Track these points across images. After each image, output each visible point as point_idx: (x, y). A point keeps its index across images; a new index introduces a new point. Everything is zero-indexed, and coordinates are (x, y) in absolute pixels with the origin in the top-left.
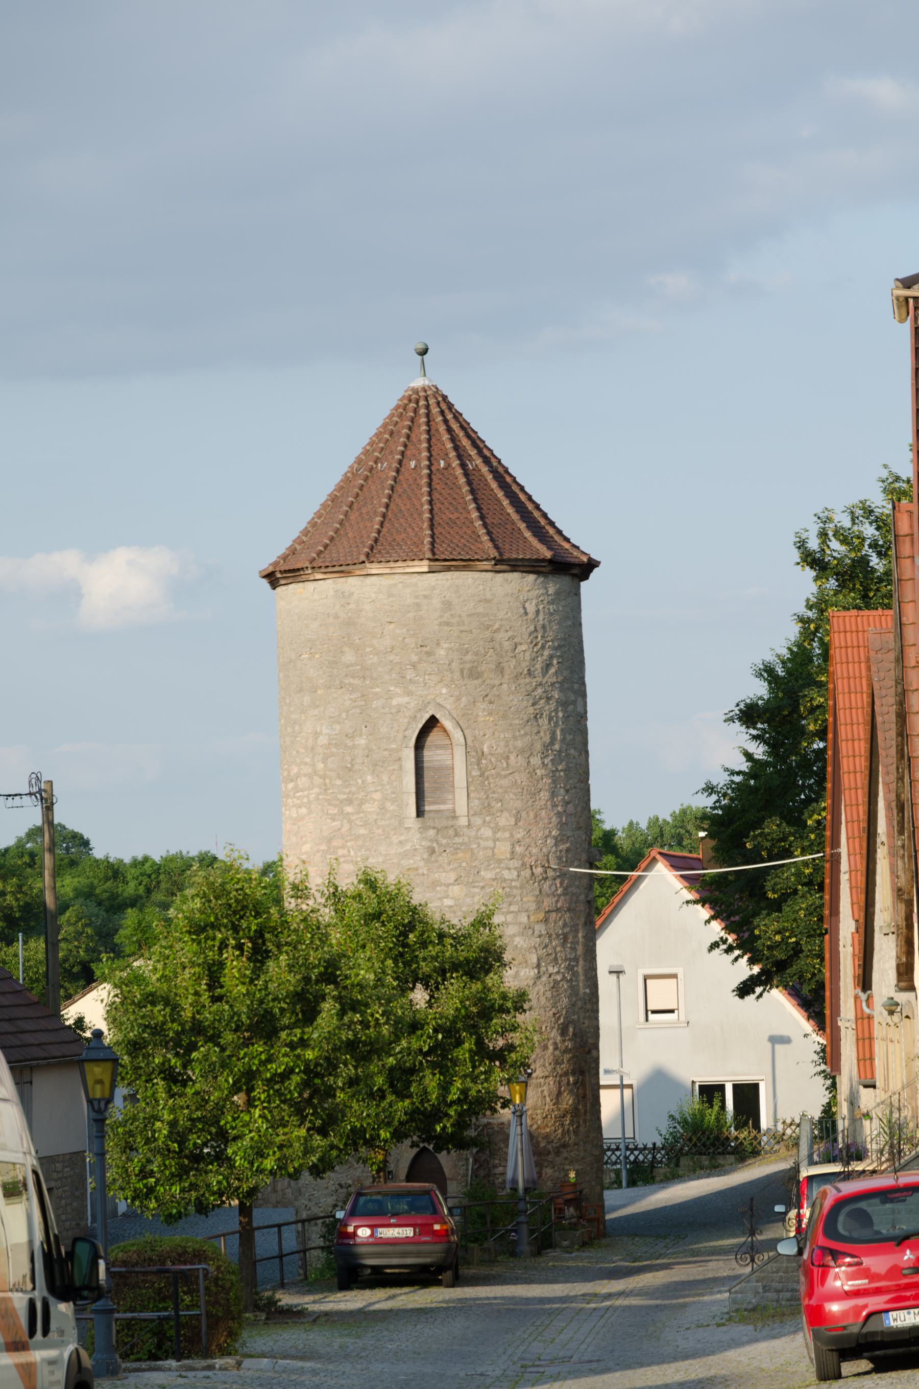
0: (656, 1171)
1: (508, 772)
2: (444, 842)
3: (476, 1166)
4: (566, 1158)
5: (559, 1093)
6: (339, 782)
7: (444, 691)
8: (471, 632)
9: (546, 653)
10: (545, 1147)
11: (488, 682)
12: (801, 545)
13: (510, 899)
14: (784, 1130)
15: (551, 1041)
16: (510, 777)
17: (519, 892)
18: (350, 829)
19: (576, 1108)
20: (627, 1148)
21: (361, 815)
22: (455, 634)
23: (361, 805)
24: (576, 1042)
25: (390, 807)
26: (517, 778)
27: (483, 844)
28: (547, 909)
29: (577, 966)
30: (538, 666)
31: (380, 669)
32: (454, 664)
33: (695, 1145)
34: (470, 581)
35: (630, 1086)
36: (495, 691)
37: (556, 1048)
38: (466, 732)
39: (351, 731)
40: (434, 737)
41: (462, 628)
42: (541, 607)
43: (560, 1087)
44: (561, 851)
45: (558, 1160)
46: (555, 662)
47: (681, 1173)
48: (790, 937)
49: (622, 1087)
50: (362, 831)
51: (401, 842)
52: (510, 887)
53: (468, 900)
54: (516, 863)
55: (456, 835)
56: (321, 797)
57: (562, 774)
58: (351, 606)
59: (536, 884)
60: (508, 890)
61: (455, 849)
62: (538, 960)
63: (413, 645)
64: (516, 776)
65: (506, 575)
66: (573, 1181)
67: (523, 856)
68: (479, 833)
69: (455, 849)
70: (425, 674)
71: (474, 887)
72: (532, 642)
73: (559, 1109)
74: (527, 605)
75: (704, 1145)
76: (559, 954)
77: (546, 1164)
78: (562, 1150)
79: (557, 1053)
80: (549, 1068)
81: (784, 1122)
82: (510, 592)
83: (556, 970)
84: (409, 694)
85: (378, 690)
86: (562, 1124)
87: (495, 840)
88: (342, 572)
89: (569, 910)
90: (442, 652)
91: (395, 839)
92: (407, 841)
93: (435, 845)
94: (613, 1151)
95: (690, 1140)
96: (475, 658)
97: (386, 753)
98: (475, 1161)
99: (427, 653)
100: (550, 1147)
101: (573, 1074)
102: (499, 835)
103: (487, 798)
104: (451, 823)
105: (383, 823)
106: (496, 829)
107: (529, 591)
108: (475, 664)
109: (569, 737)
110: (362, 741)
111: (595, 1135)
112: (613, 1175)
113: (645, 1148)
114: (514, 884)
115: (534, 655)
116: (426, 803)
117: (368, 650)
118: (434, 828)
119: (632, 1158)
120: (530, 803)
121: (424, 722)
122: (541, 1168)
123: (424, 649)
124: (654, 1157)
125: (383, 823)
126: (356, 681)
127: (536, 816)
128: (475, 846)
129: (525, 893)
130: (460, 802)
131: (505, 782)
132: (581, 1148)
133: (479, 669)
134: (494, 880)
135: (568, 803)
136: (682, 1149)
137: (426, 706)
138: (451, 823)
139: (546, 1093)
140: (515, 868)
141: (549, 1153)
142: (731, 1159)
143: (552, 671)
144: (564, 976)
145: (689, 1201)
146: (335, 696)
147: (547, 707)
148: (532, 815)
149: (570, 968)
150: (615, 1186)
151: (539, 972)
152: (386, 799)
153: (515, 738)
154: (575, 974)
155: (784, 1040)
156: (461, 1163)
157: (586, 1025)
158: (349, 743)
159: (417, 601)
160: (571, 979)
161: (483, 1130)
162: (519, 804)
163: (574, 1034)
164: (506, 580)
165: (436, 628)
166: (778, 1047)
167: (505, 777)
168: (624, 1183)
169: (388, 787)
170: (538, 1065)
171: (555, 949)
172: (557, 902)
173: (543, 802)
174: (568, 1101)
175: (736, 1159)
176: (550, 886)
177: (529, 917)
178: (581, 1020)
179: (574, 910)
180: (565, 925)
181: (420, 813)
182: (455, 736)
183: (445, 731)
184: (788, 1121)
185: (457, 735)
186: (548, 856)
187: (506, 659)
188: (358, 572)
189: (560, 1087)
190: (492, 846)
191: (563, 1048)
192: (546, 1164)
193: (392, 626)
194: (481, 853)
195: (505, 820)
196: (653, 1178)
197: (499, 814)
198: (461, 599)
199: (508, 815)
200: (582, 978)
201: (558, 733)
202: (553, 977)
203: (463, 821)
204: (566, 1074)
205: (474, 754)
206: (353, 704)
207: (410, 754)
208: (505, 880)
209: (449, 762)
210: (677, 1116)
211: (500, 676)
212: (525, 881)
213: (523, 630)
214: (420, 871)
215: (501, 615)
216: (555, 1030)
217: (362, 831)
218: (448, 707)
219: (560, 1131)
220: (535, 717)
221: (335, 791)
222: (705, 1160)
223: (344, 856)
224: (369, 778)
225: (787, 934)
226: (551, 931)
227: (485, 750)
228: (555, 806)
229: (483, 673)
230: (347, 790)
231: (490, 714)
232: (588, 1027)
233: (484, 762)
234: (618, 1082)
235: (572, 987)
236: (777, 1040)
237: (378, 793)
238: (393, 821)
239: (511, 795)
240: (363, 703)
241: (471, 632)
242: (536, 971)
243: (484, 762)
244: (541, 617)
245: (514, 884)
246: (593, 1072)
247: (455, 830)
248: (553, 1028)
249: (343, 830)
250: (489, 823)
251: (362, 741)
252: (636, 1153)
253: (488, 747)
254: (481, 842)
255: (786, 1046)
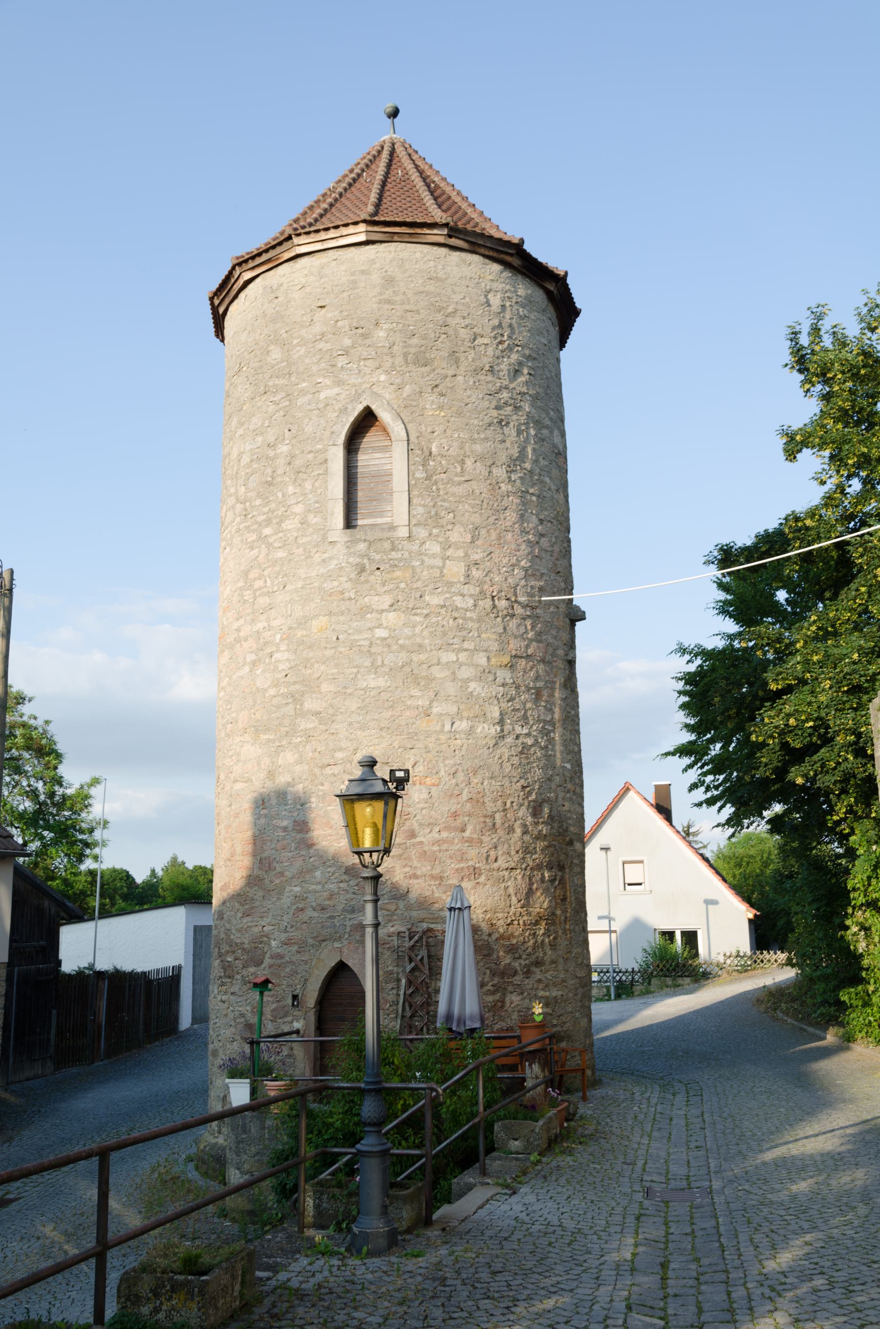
0: (634, 988)
1: (463, 479)
2: (377, 557)
3: (411, 991)
4: (540, 981)
5: (530, 892)
6: (258, 502)
7: (383, 378)
8: (418, 312)
9: (514, 357)
10: (509, 964)
11: (439, 371)
12: (794, 335)
13: (464, 633)
14: (725, 960)
15: (518, 822)
16: (465, 485)
17: (476, 625)
18: (267, 554)
19: (553, 914)
20: (614, 972)
21: (280, 535)
22: (398, 314)
23: (279, 523)
24: (552, 828)
25: (313, 519)
26: (475, 487)
27: (428, 561)
28: (514, 653)
29: (553, 731)
30: (504, 367)
31: (307, 361)
32: (396, 348)
33: (662, 970)
34: (418, 255)
35: (615, 932)
36: (448, 382)
37: (525, 832)
38: (409, 426)
39: (273, 440)
40: (370, 439)
41: (408, 307)
42: (508, 304)
43: (531, 884)
44: (532, 587)
45: (529, 983)
46: (525, 371)
47: (652, 990)
48: (807, 721)
49: (611, 932)
50: (281, 554)
51: (324, 561)
52: (464, 619)
53: (407, 631)
54: (472, 589)
55: (393, 549)
56: (241, 527)
57: (534, 498)
58: (279, 299)
59: (499, 619)
60: (461, 621)
61: (391, 566)
62: (501, 714)
63: (347, 328)
64: (474, 485)
65: (464, 255)
66: (538, 1019)
67: (481, 583)
68: (424, 547)
69: (391, 566)
70: (360, 360)
71: (416, 614)
72: (495, 338)
73: (529, 914)
74: (490, 296)
75: (668, 970)
76: (529, 713)
77: (510, 988)
78: (533, 969)
79: (527, 838)
80: (516, 858)
81: (725, 955)
82: (469, 275)
83: (525, 731)
84: (339, 383)
85: (304, 385)
86: (534, 934)
87: (445, 558)
88: (269, 261)
89: (543, 661)
90: (382, 334)
91: (317, 558)
92: (331, 558)
93: (366, 561)
94: (605, 973)
95: (658, 966)
96: (423, 342)
97: (310, 456)
98: (409, 983)
99: (362, 335)
100: (516, 964)
101: (550, 868)
102: (449, 553)
103: (434, 506)
104: (386, 534)
105: (305, 540)
106: (447, 545)
107: (492, 280)
108: (423, 348)
109: (543, 463)
110: (284, 449)
111: (579, 950)
112: (605, 990)
113: (627, 972)
114: (468, 614)
115: (498, 353)
116: (359, 516)
117: (295, 342)
118: (365, 541)
119: (618, 978)
120: (492, 520)
121: (356, 414)
122: (504, 995)
123: (360, 331)
124: (633, 978)
125: (305, 540)
126: (280, 382)
127: (499, 538)
128: (418, 563)
129: (483, 628)
130: (398, 511)
131: (460, 490)
132: (561, 967)
133: (428, 355)
134: (442, 607)
135: (542, 535)
136: (652, 973)
137: (358, 396)
138: (386, 534)
139: (511, 891)
140: (471, 596)
141: (515, 973)
142: (688, 980)
143: (521, 379)
144: (536, 740)
145: (672, 1019)
146: (259, 404)
147: (515, 417)
148: (494, 535)
149: (545, 733)
150: (607, 998)
151: (502, 731)
152: (309, 511)
153: (473, 441)
154: (551, 741)
155: (714, 902)
156: (390, 986)
157: (566, 808)
158: (271, 453)
159: (354, 278)
160: (546, 747)
161: (421, 938)
162: (476, 519)
163: (551, 817)
164: (464, 261)
165: (375, 306)
166: (710, 906)
167: (459, 484)
168: (613, 997)
169: (311, 496)
170: (500, 853)
171: (524, 704)
172: (527, 647)
173: (509, 524)
174: (542, 903)
175: (692, 981)
176: (519, 626)
177: (488, 659)
178: (560, 802)
179: (549, 663)
180: (537, 678)
181: (349, 524)
182: (395, 429)
183: (385, 430)
184: (728, 954)
185: (397, 429)
186: (515, 588)
187: (462, 349)
188: (287, 256)
189: (531, 884)
190: (441, 565)
191: (536, 832)
192: (510, 988)
193: (324, 310)
194: (425, 573)
195: (457, 535)
196: (633, 993)
197: (450, 527)
198: (407, 275)
199: (462, 529)
200: (559, 748)
201: (529, 450)
202: (521, 740)
203: (403, 532)
204: (539, 867)
205: (419, 452)
206: (277, 408)
207: (338, 455)
208: (457, 609)
209: (389, 467)
210: (648, 950)
211: (454, 367)
212: (483, 613)
213: (485, 324)
214: (347, 595)
215: (457, 297)
216: (524, 808)
217: (281, 554)
218: (387, 396)
219: (531, 943)
220: (500, 422)
221: (255, 513)
222: (669, 981)
223: (260, 589)
224: (291, 489)
225: (803, 718)
226: (519, 681)
227: (434, 450)
228: (524, 532)
229: (433, 360)
230: (266, 510)
231: (441, 408)
232: (569, 811)
233: (431, 463)
234: (608, 929)
235: (548, 757)
236: (708, 902)
237: (300, 505)
238: (315, 536)
239: (467, 507)
240: (287, 403)
241: (418, 312)
242: (499, 729)
243: (431, 463)
244: (508, 315)
245: (468, 614)
246: (577, 869)
247: (392, 542)
248: (522, 805)
249: (261, 557)
250: (437, 536)
251: (284, 449)
252: (621, 974)
253: (437, 447)
254: (426, 559)
255: (715, 906)
